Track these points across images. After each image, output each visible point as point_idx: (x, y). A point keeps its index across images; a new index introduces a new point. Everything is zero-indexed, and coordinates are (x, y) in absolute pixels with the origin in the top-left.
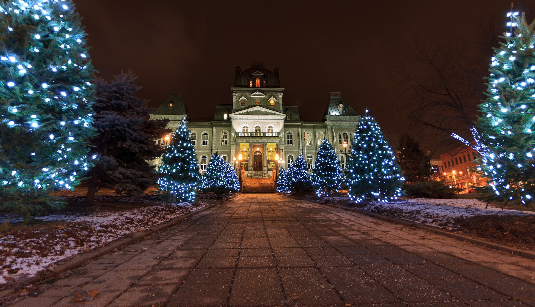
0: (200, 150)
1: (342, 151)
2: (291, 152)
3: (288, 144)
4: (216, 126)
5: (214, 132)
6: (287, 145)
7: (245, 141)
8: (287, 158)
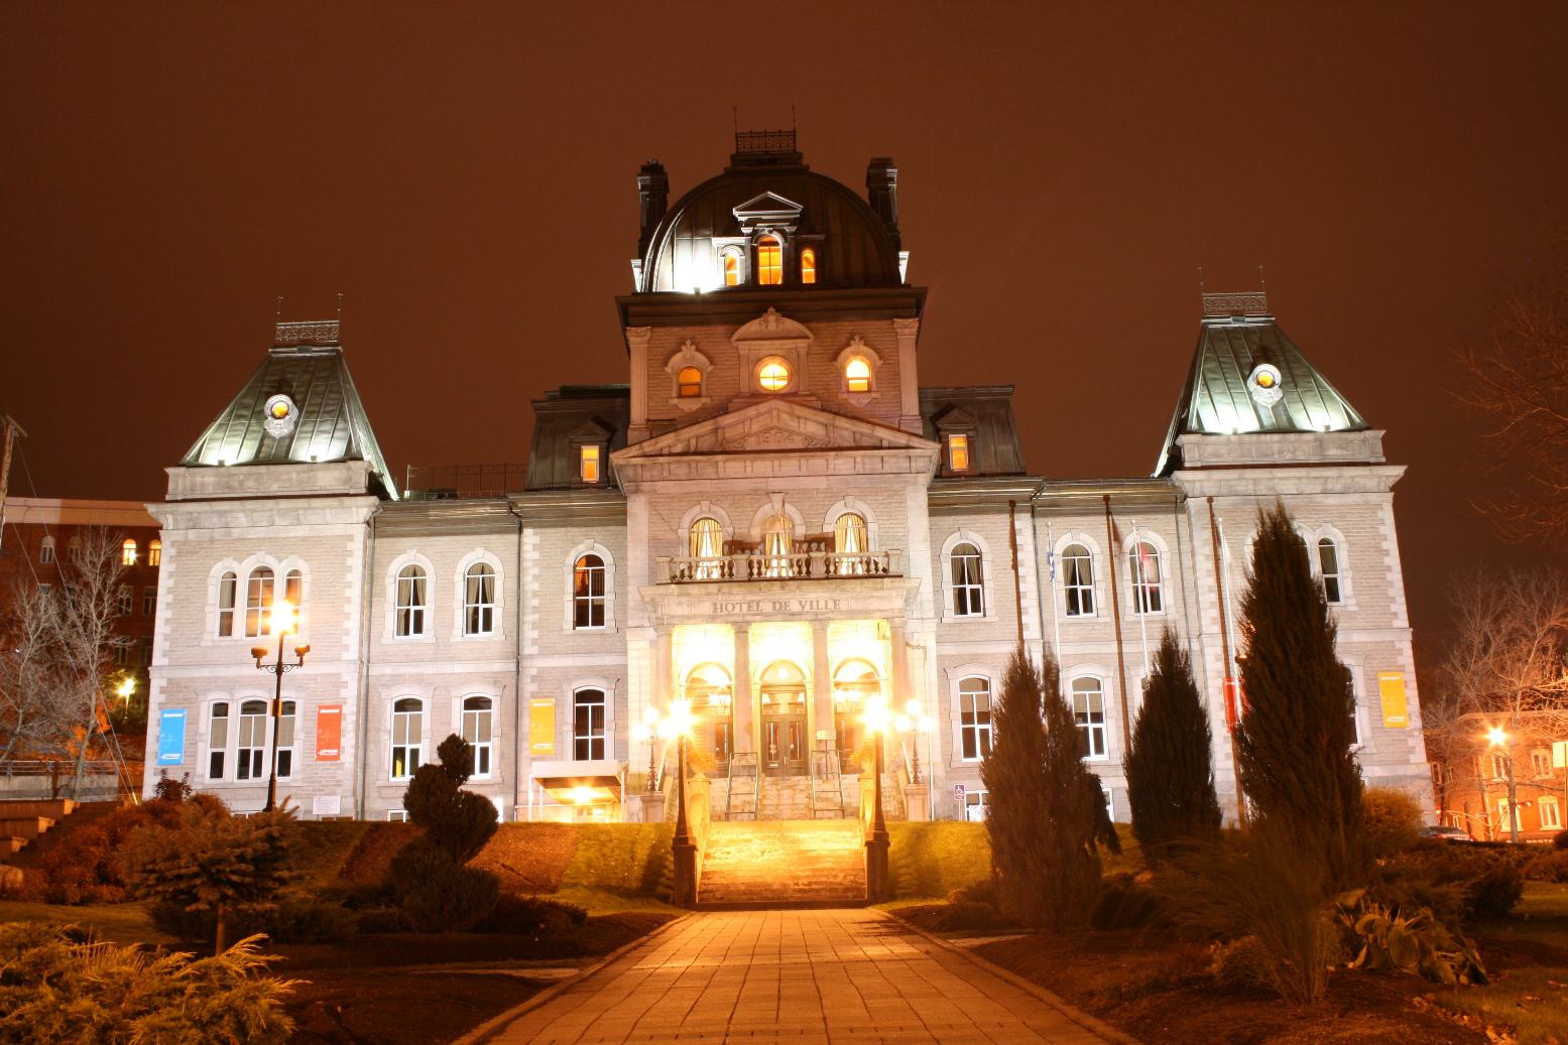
0: (452, 659)
1: (257, 653)
2: (974, 659)
3: (962, 609)
4: (541, 521)
5: (530, 554)
6: (950, 615)
7: (706, 608)
8: (956, 694)
